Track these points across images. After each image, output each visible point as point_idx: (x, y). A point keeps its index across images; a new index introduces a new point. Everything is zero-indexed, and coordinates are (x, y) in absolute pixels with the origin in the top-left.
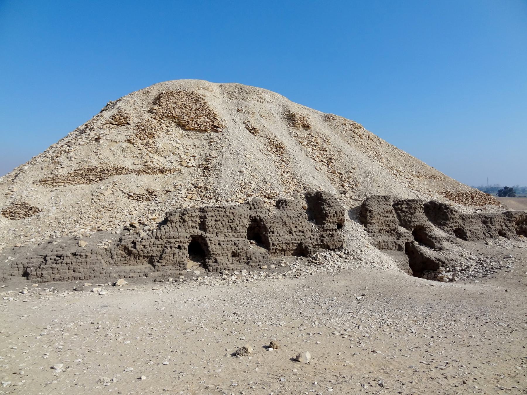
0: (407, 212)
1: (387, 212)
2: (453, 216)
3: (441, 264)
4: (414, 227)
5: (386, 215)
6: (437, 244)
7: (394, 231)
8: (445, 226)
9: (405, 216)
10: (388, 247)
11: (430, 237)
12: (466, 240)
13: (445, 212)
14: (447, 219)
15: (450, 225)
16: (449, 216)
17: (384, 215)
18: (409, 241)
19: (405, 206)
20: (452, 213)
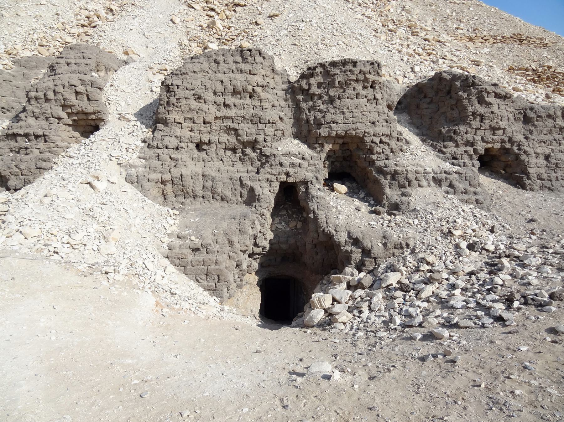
0: (320, 97)
1: (235, 92)
2: (481, 109)
3: (357, 256)
4: (328, 139)
5: (230, 100)
6: (392, 194)
7: (254, 149)
8: (451, 139)
9: (311, 109)
10: (214, 193)
11: (380, 171)
12: (523, 187)
13: (459, 100)
14: (462, 118)
15: (470, 137)
16: (470, 110)
17: (220, 100)
18: (290, 180)
19: (320, 79)
20: (481, 101)
